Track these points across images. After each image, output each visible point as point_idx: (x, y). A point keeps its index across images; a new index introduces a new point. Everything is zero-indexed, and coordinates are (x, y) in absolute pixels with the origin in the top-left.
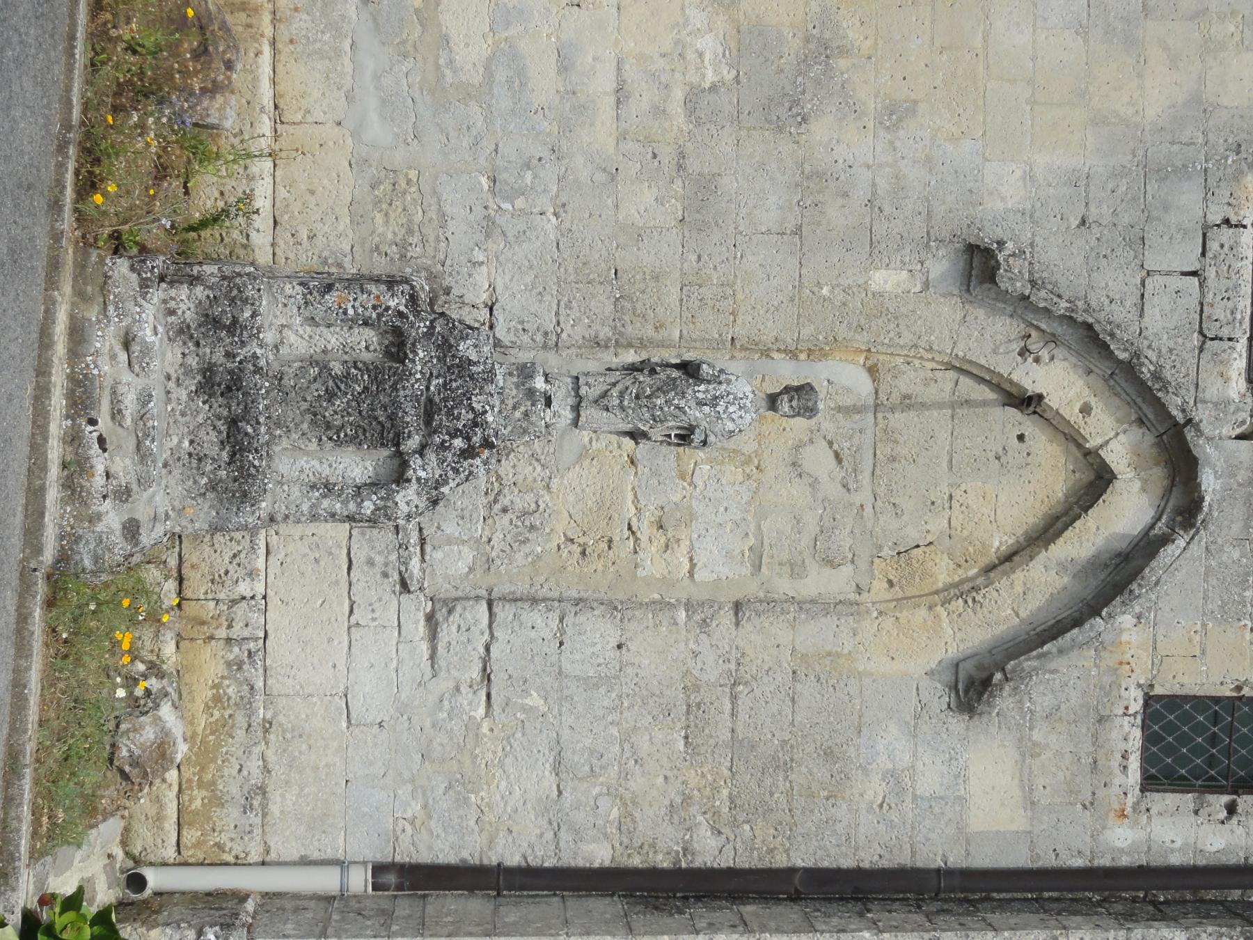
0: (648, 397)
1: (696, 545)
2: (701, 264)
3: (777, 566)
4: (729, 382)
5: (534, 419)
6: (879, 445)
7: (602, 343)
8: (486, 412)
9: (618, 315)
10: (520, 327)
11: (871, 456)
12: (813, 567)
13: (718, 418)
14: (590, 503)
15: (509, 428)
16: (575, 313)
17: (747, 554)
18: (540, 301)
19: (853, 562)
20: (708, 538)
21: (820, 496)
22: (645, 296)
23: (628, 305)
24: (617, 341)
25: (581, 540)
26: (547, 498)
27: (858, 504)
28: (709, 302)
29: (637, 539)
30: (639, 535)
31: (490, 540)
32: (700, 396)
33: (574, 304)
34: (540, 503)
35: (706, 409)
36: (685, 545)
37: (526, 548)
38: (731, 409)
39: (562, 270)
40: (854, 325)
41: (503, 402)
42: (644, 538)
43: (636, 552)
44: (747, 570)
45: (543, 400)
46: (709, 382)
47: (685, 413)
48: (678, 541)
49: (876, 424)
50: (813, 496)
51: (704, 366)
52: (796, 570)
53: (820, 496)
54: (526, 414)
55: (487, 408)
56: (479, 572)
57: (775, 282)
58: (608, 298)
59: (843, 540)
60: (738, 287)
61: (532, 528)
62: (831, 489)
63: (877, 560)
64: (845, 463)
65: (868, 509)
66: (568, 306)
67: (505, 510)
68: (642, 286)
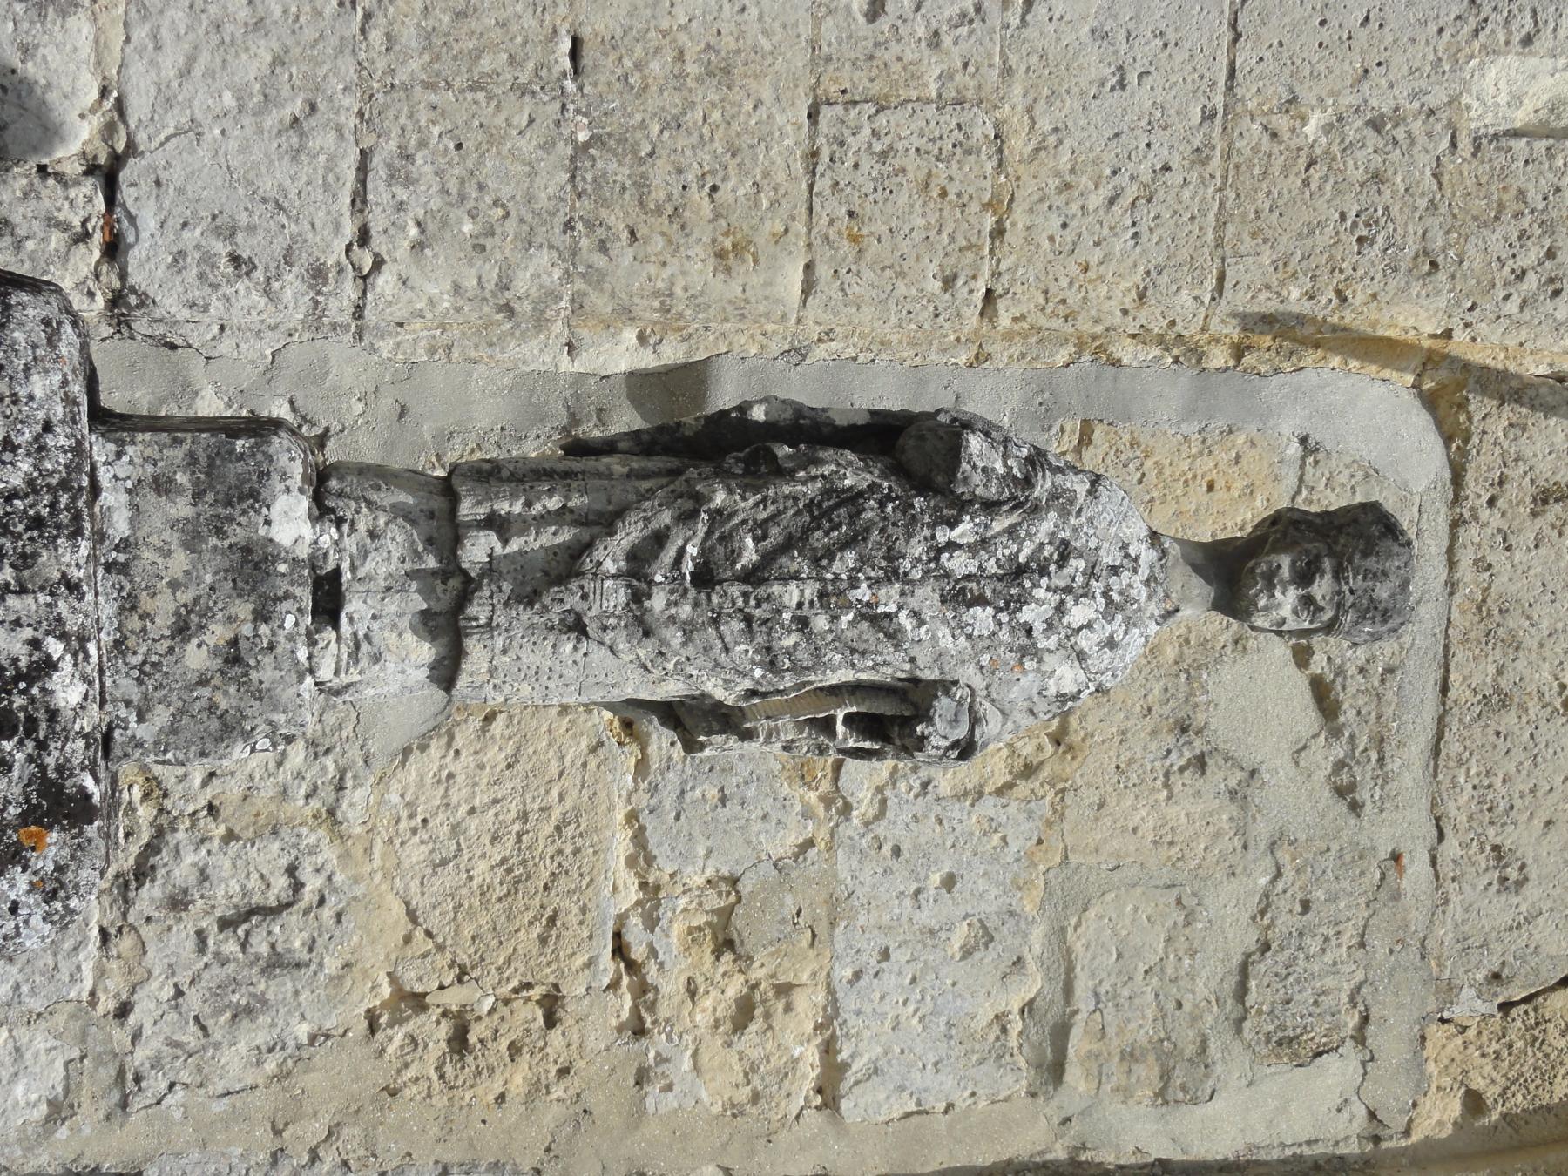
0: (753, 576)
1: (848, 1002)
2: (884, 24)
3: (1114, 1064)
4: (1061, 501)
5: (266, 673)
6: (1459, 655)
7: (525, 308)
8: (49, 665)
9: (584, 207)
10: (221, 249)
11: (1432, 693)
12: (1231, 1062)
13: (1023, 652)
14: (482, 867)
15: (161, 716)
16: (424, 199)
17: (1016, 1026)
18: (296, 154)
19: (1360, 1039)
20: (889, 980)
21: (1262, 830)
22: (682, 141)
23: (621, 172)
24: (578, 305)
25: (454, 998)
26: (329, 854)
27: (1384, 852)
28: (911, 163)
29: (642, 989)
30: (652, 972)
31: (123, 1011)
32: (959, 564)
33: (422, 165)
34: (305, 874)
35: (982, 618)
36: (808, 1004)
37: (257, 1033)
38: (1078, 614)
39: (376, 36)
40: (1410, 252)
41: (129, 604)
42: (670, 986)
43: (640, 1031)
44: (1016, 1080)
45: (305, 596)
46: (991, 507)
47: (895, 636)
48: (784, 990)
49: (1452, 587)
50: (1241, 831)
51: (975, 443)
52: (1178, 1078)
53: (1262, 830)
54: (233, 657)
55: (55, 648)
56: (89, 1115)
57: (1143, 98)
58: (548, 146)
59: (1329, 974)
60: (1012, 111)
61: (277, 963)
62: (1295, 795)
63: (1436, 1033)
64: (1347, 715)
65: (1417, 868)
66: (401, 174)
67: (178, 903)
68: (672, 101)
